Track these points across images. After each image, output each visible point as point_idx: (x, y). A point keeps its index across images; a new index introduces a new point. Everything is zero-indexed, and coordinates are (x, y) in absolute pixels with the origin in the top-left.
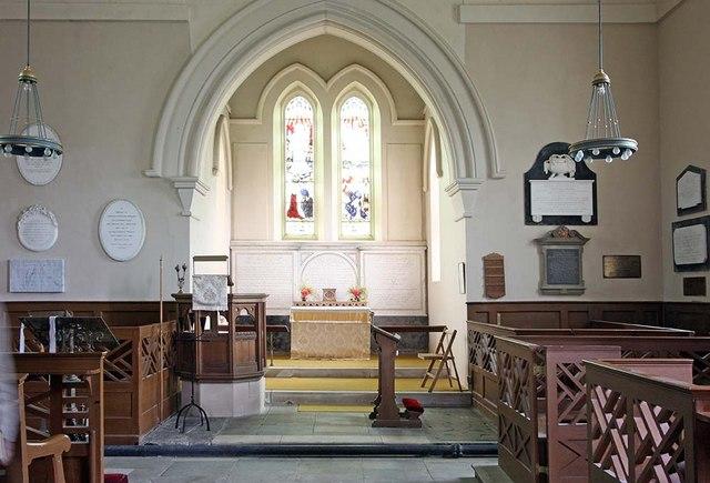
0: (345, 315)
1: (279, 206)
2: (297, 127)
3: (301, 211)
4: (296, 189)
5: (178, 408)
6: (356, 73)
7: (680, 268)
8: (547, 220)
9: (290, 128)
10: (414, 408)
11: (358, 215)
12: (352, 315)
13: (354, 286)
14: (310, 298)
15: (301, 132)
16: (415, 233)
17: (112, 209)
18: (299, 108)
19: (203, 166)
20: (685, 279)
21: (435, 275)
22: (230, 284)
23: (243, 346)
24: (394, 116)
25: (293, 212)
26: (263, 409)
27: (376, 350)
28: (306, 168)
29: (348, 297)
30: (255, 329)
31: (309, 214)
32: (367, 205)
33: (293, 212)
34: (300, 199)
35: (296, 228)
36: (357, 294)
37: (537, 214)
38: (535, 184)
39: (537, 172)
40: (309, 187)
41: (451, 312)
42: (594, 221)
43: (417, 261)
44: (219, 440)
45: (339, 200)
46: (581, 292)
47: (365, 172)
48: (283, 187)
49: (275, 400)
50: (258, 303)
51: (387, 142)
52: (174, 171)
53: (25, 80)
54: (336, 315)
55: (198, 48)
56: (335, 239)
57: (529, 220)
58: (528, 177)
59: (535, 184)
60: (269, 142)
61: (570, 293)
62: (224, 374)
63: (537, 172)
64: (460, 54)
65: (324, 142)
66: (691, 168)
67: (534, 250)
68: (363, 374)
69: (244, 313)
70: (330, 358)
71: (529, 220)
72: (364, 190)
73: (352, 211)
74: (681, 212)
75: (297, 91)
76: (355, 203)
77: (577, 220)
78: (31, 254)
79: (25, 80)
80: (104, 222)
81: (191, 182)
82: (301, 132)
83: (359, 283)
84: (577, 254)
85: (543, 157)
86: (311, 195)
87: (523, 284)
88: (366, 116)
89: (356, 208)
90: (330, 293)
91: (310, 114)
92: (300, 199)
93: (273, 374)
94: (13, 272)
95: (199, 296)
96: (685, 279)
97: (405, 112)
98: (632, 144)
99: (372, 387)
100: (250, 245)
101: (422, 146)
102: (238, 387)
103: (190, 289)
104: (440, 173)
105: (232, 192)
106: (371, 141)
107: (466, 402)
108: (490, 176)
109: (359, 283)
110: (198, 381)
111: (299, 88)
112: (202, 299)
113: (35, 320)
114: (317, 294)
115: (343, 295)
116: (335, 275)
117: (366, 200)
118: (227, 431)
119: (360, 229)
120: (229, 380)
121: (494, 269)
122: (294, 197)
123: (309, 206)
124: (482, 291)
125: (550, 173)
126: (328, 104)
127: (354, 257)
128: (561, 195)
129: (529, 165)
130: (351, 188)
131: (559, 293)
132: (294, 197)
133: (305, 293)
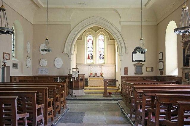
0: (99, 78)
1: (86, 57)
2: (90, 41)
3: (90, 58)
4: (89, 53)
5: (70, 94)
6: (102, 30)
7: (160, 70)
8: (136, 61)
9: (88, 41)
10: (110, 93)
11: (102, 59)
12: (101, 79)
13: (101, 72)
14: (92, 75)
15: (91, 42)
16: (113, 62)
17: (57, 59)
18: (90, 37)
19: (72, 52)
20: (160, 72)
21: (117, 71)
22: (79, 73)
23: (81, 84)
24: (109, 39)
25: (89, 58)
26: (84, 95)
27: (104, 86)
28: (92, 49)
29: (99, 75)
30: (83, 81)
31: (92, 58)
32: (103, 57)
33: (89, 58)
34: (90, 55)
35: (90, 61)
36: (101, 74)
37: (134, 60)
38: (134, 54)
39: (134, 52)
40: (92, 53)
41: (119, 78)
42: (145, 61)
43: (114, 68)
44: (77, 98)
45: (98, 56)
46: (142, 74)
47: (103, 50)
48: (87, 53)
49: (86, 93)
50: (83, 76)
51: (108, 44)
52: (68, 52)
53: (46, 39)
54: (97, 78)
55: (73, 29)
56: (97, 63)
57: (133, 61)
58: (133, 53)
59: (134, 54)
60: (84, 44)
61: (140, 74)
62: (78, 88)
63: (134, 52)
64: (120, 31)
65: (94, 44)
66: (161, 52)
67: (134, 66)
68: (102, 89)
69: (81, 78)
70: (96, 87)
71: (133, 61)
72: (103, 53)
73: (101, 58)
74: (160, 60)
75: (90, 34)
76: (101, 56)
77: (142, 61)
78: (42, 67)
79: (46, 39)
80: (55, 61)
81: (71, 54)
82: (91, 42)
83: (102, 72)
84: (141, 67)
85: (135, 49)
86: (92, 54)
87: (132, 72)
88: (104, 39)
89: (102, 57)
90: (96, 74)
91: (92, 38)
92: (90, 55)
93: (85, 89)
94: (39, 70)
95: (73, 75)
96: (160, 72)
97: (111, 38)
98: (146, 50)
99: (103, 91)
100: (80, 64)
101: (115, 45)
102: (80, 90)
103: (71, 73)
104: (117, 51)
105: (77, 54)
106: (104, 44)
107: (121, 93)
108: (126, 53)
109: (102, 72)
110: (73, 89)
111: (90, 33)
112: (74, 75)
113: (56, 78)
114: (94, 73)
115: (98, 74)
116: (98, 71)
117: (104, 55)
118: (78, 97)
119: (102, 61)
120: (78, 89)
121: (126, 70)
122: (89, 55)
123: (92, 57)
124: (134, 71)
125: (137, 52)
126: (95, 36)
127: (101, 67)
128: (139, 56)
129: (133, 51)
130: (100, 53)
131: (138, 74)
132: (89, 55)
133: (91, 74)
